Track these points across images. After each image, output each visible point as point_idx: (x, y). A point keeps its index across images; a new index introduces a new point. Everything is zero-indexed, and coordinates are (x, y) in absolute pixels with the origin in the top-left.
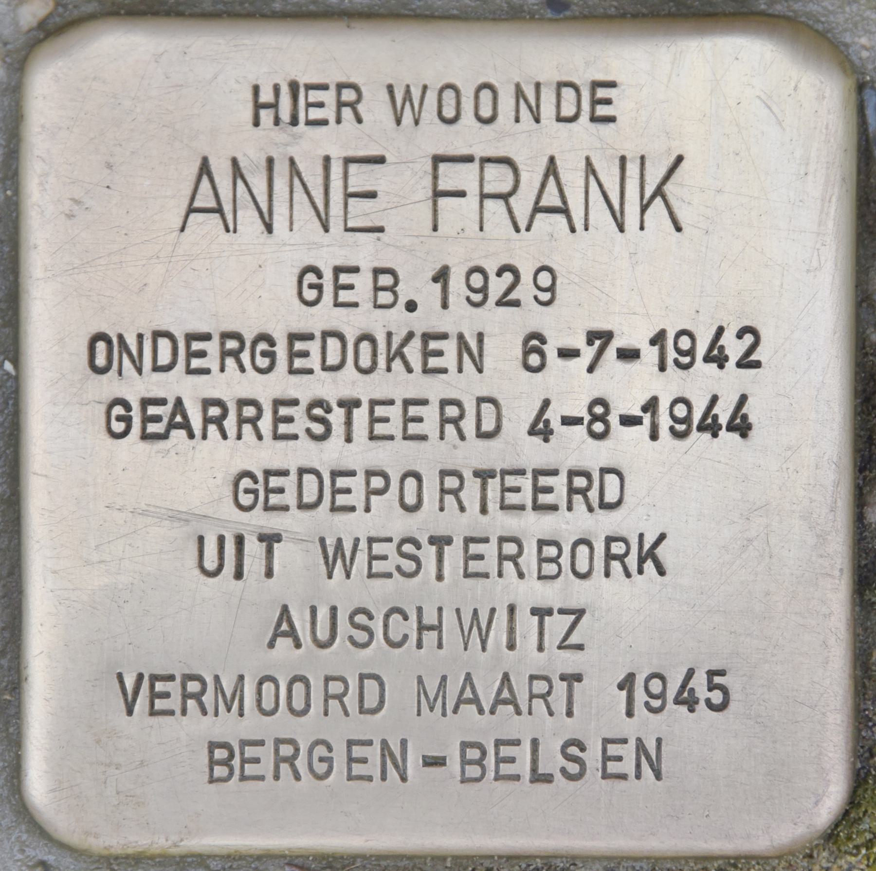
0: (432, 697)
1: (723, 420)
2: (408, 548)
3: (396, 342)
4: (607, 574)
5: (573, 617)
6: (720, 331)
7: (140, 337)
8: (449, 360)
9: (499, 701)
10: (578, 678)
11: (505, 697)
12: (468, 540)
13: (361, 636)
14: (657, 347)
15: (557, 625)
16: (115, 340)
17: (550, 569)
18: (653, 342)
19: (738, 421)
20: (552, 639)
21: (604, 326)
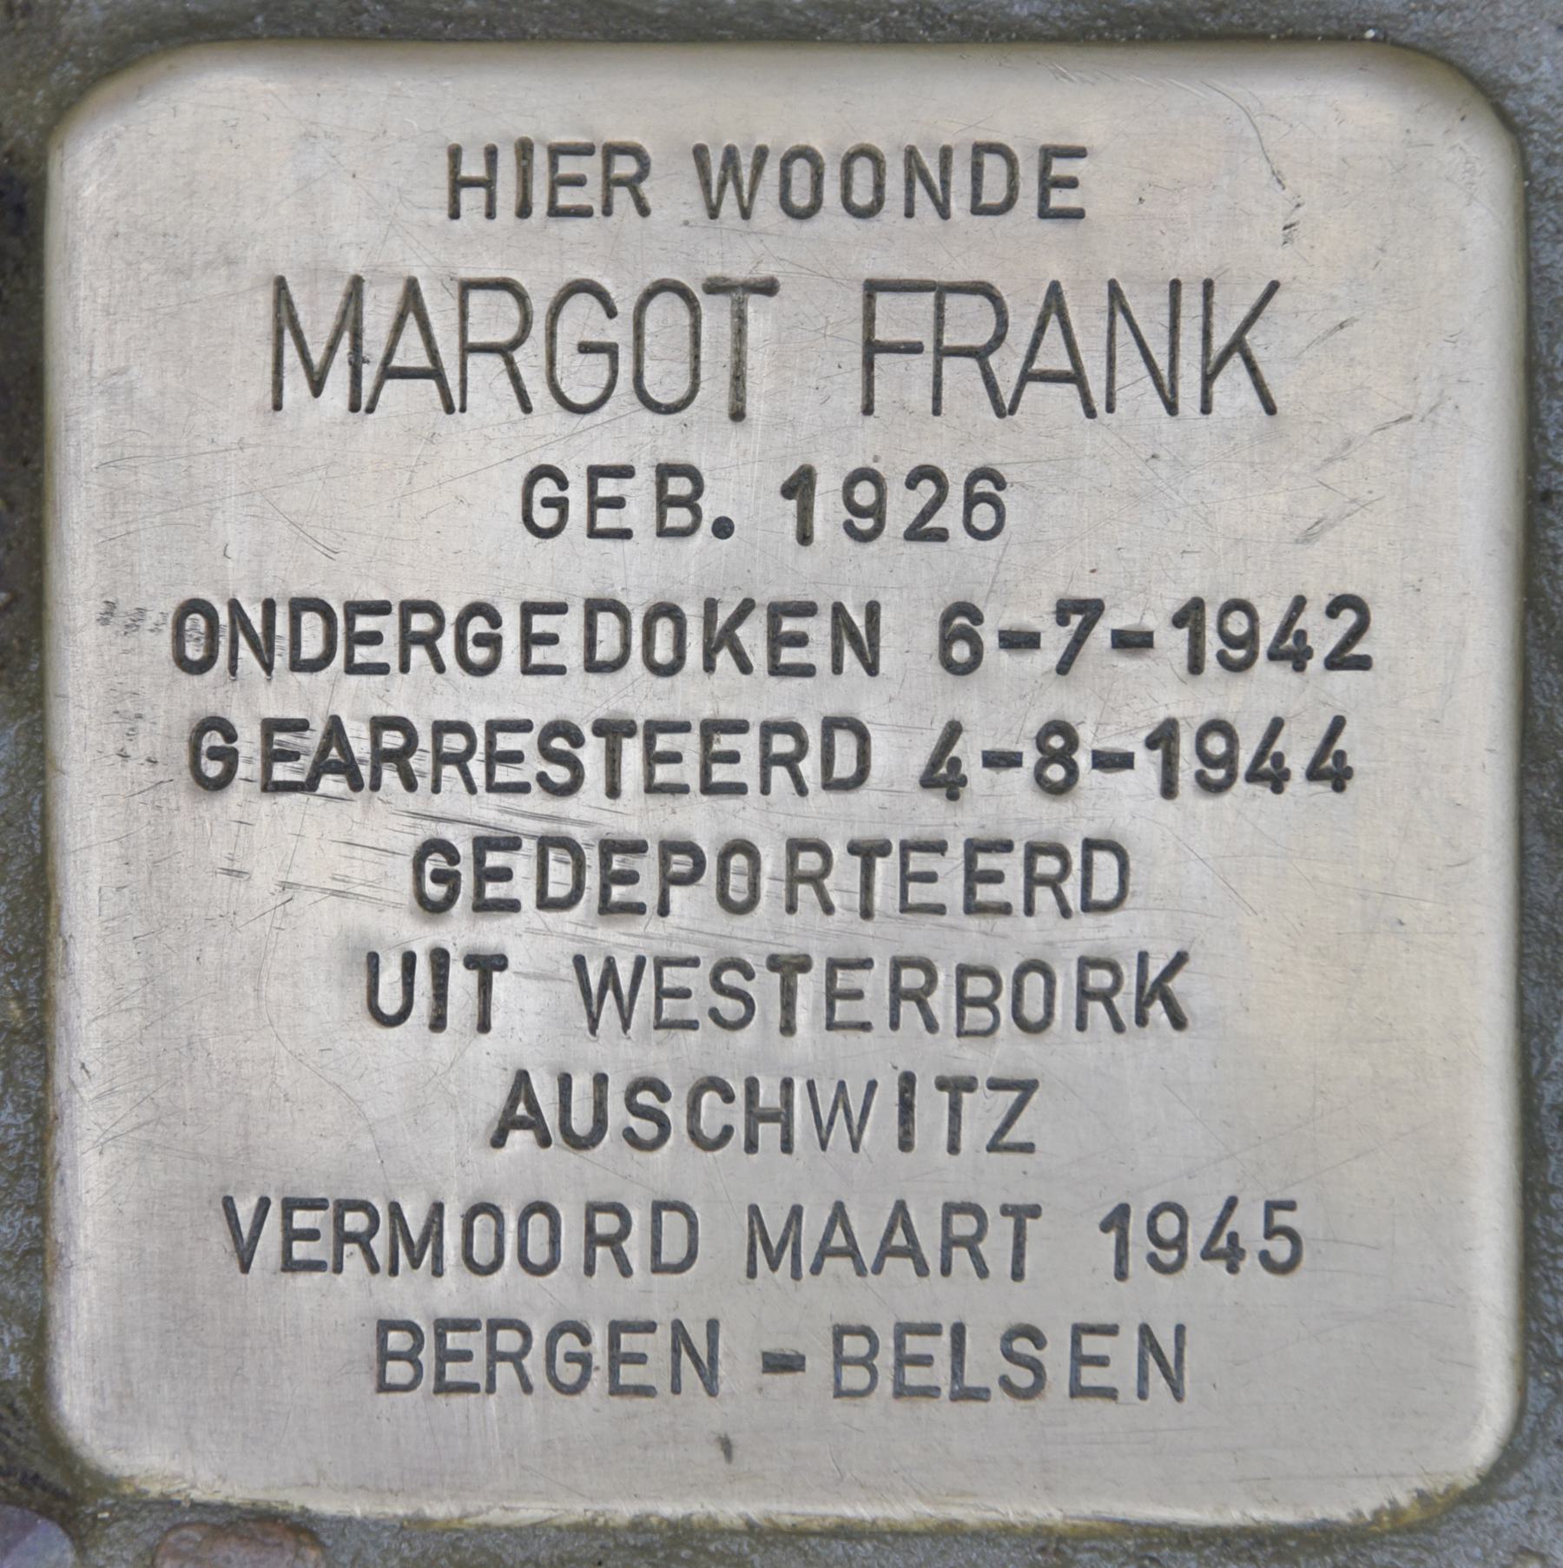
0: (774, 1242)
1: (1297, 763)
2: (731, 978)
3: (723, 615)
4: (1081, 1025)
5: (1015, 1094)
6: (1299, 604)
7: (269, 607)
8: (818, 653)
9: (887, 1250)
10: (1035, 1211)
11: (898, 1238)
12: (834, 965)
13: (646, 1129)
14: (1185, 632)
15: (983, 1111)
16: (224, 618)
17: (978, 1017)
18: (1178, 621)
19: (1329, 762)
20: (975, 1131)
21: (1086, 592)
